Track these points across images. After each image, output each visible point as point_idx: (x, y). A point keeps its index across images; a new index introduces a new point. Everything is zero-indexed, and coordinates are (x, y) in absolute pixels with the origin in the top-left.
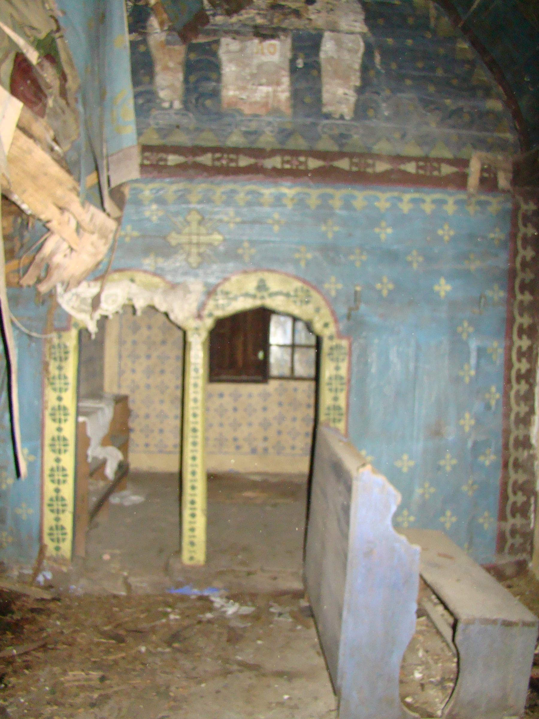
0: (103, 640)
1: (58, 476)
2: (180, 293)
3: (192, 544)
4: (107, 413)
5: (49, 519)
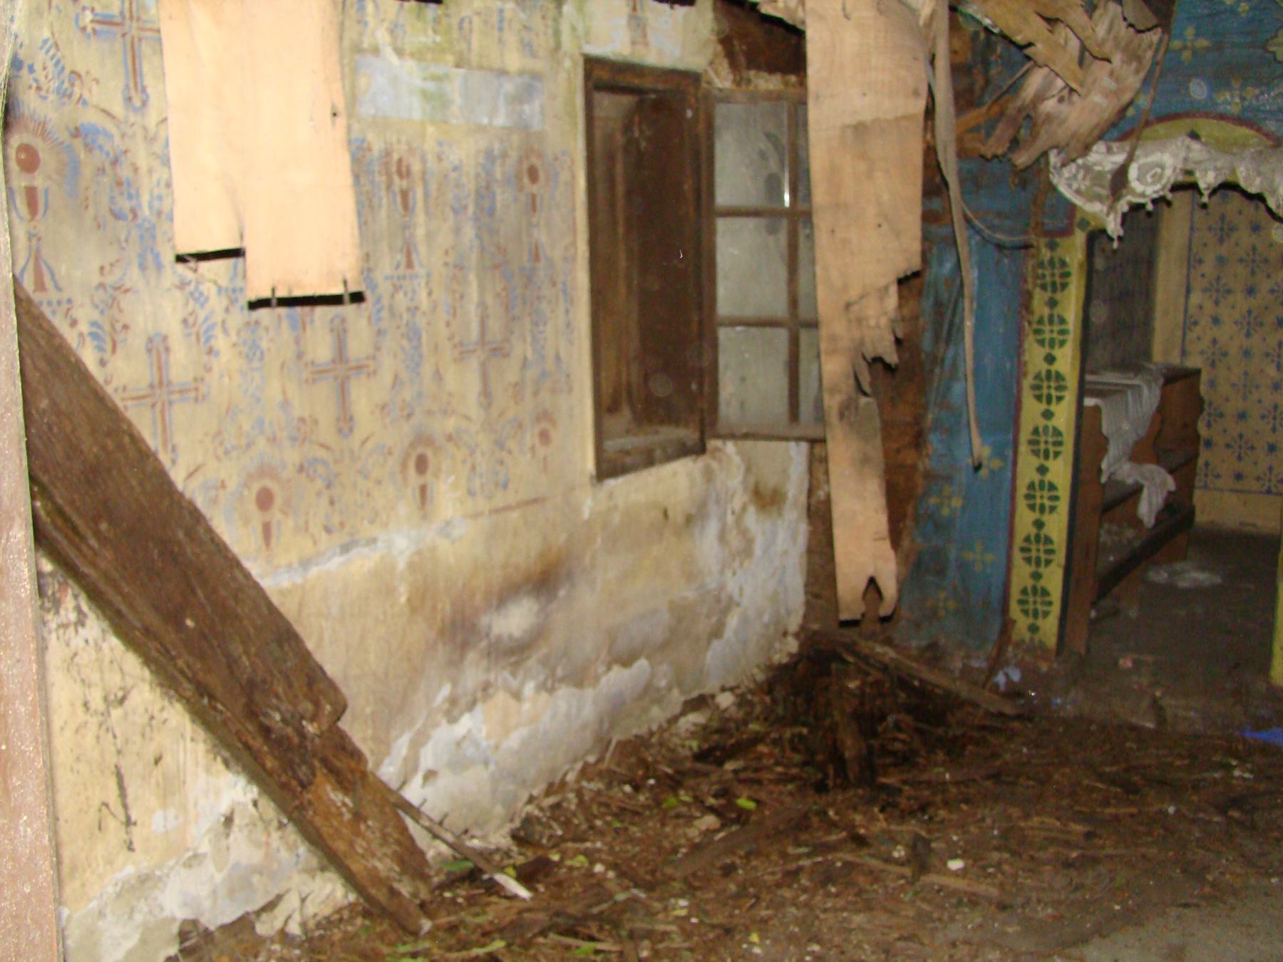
0: (1100, 785)
1: (1042, 498)
5: (1021, 575)
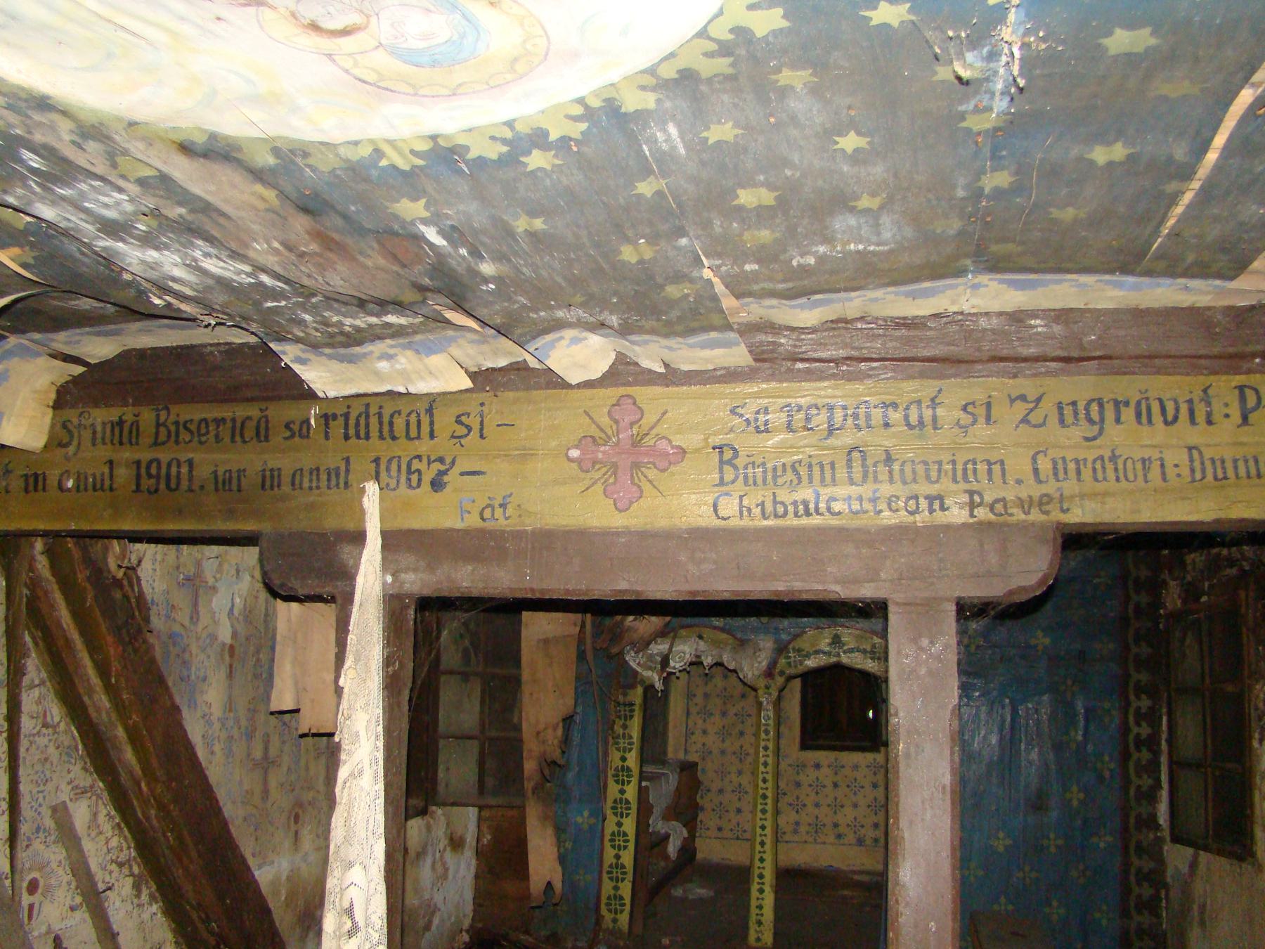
2: (750, 651)
3: (760, 923)
4: (672, 780)
5: (607, 888)
